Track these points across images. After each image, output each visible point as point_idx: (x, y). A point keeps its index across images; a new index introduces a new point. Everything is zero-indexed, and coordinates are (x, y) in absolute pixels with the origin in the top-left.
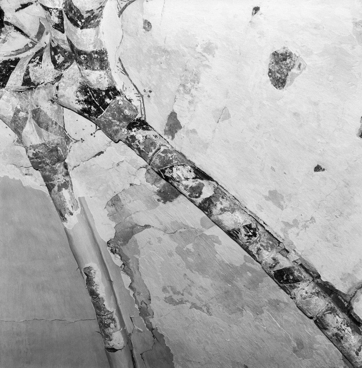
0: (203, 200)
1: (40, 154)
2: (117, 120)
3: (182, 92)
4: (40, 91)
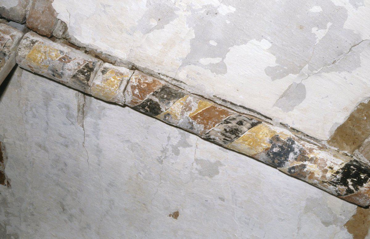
0: (284, 166)
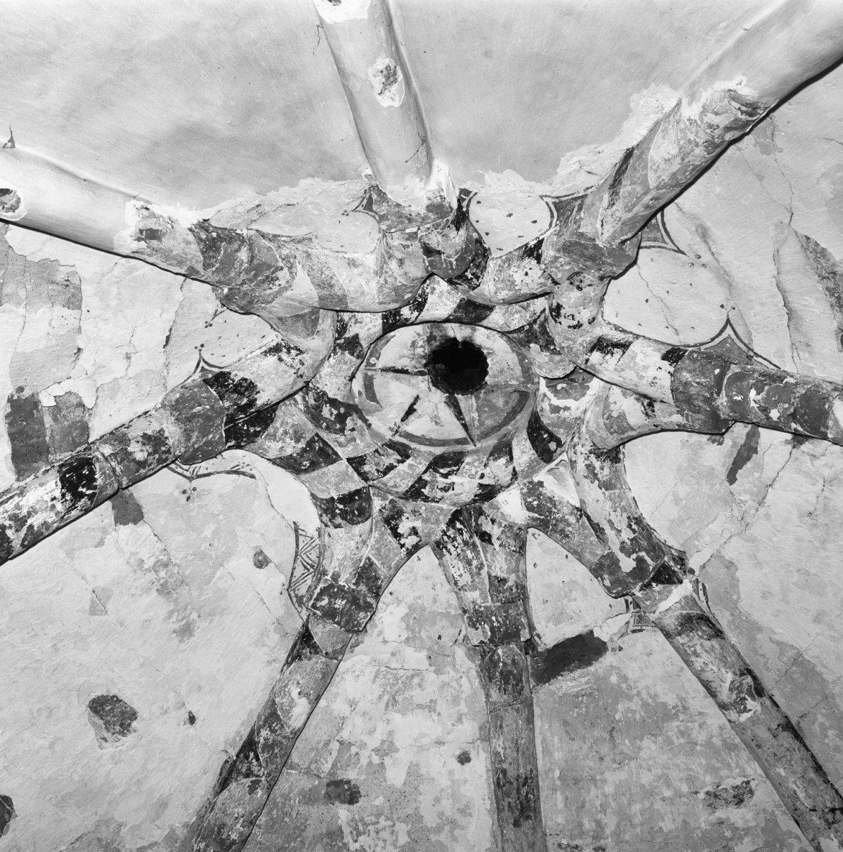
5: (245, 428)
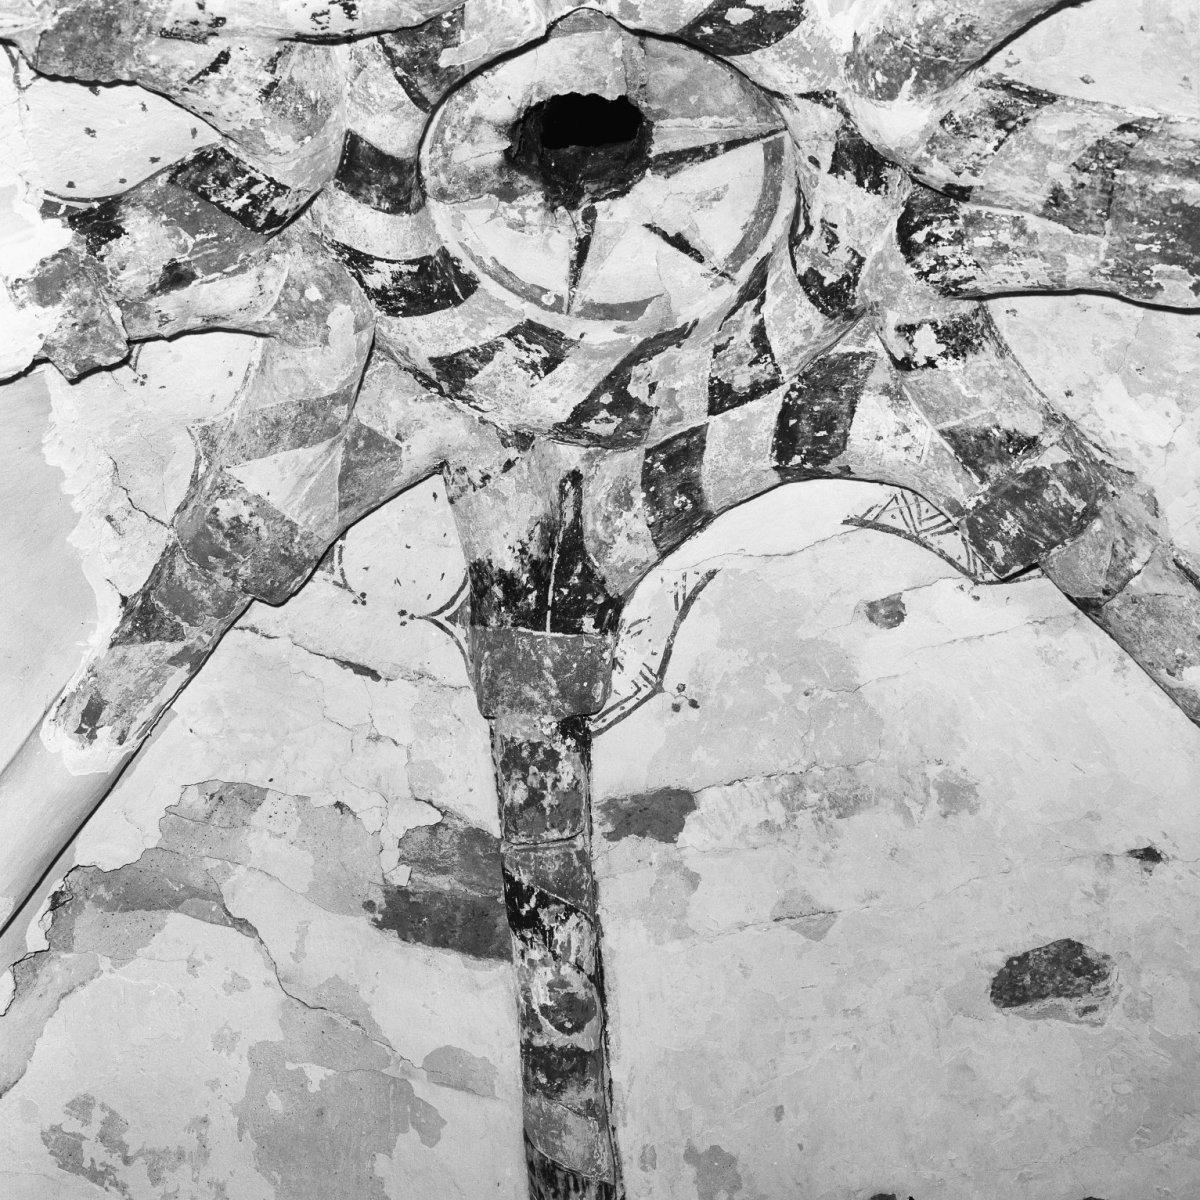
1: (249, 538)
2: (558, 683)
3: (778, 789)
4: (454, 419)
5: (565, 591)
